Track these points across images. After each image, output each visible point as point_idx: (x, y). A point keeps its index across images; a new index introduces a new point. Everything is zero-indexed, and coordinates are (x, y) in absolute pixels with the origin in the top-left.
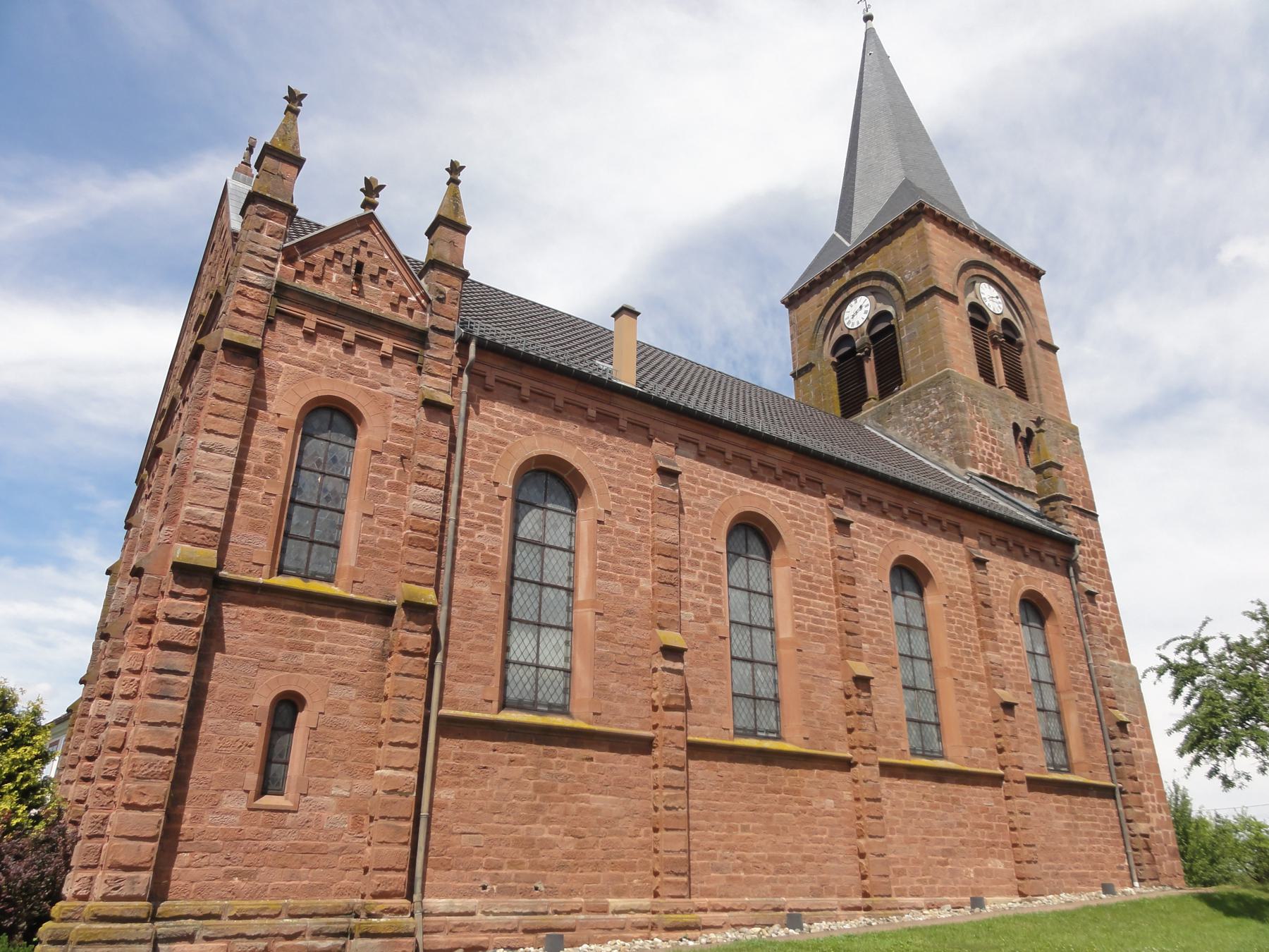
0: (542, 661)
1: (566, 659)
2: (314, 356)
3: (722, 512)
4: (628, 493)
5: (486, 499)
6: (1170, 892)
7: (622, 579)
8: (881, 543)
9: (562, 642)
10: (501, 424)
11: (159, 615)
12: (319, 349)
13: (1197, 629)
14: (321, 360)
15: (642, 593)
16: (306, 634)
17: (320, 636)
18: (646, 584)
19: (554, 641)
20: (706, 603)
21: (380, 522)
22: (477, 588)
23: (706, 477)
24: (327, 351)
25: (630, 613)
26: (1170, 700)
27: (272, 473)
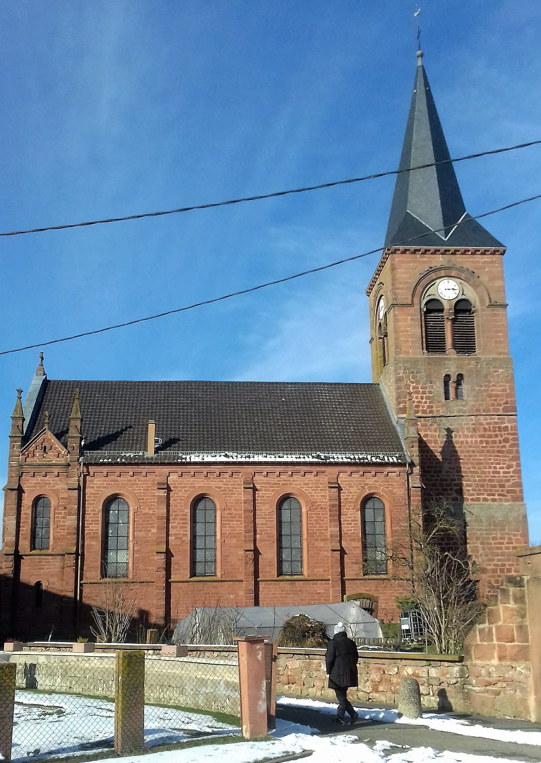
0: (207, 538)
1: (127, 559)
2: (34, 483)
3: (188, 497)
4: (147, 499)
5: (93, 514)
6: (510, 503)
7: (144, 531)
8: (273, 491)
9: (125, 554)
10: (97, 487)
11: (3, 567)
12: (36, 480)
13: (476, 216)
14: (37, 483)
15: (152, 534)
16: (41, 565)
17: (45, 565)
18: (154, 531)
19: (122, 554)
20: (180, 532)
21: (59, 529)
22: (92, 543)
23: (182, 484)
24: (38, 480)
25: (148, 541)
26: (362, 761)
27: (27, 522)
